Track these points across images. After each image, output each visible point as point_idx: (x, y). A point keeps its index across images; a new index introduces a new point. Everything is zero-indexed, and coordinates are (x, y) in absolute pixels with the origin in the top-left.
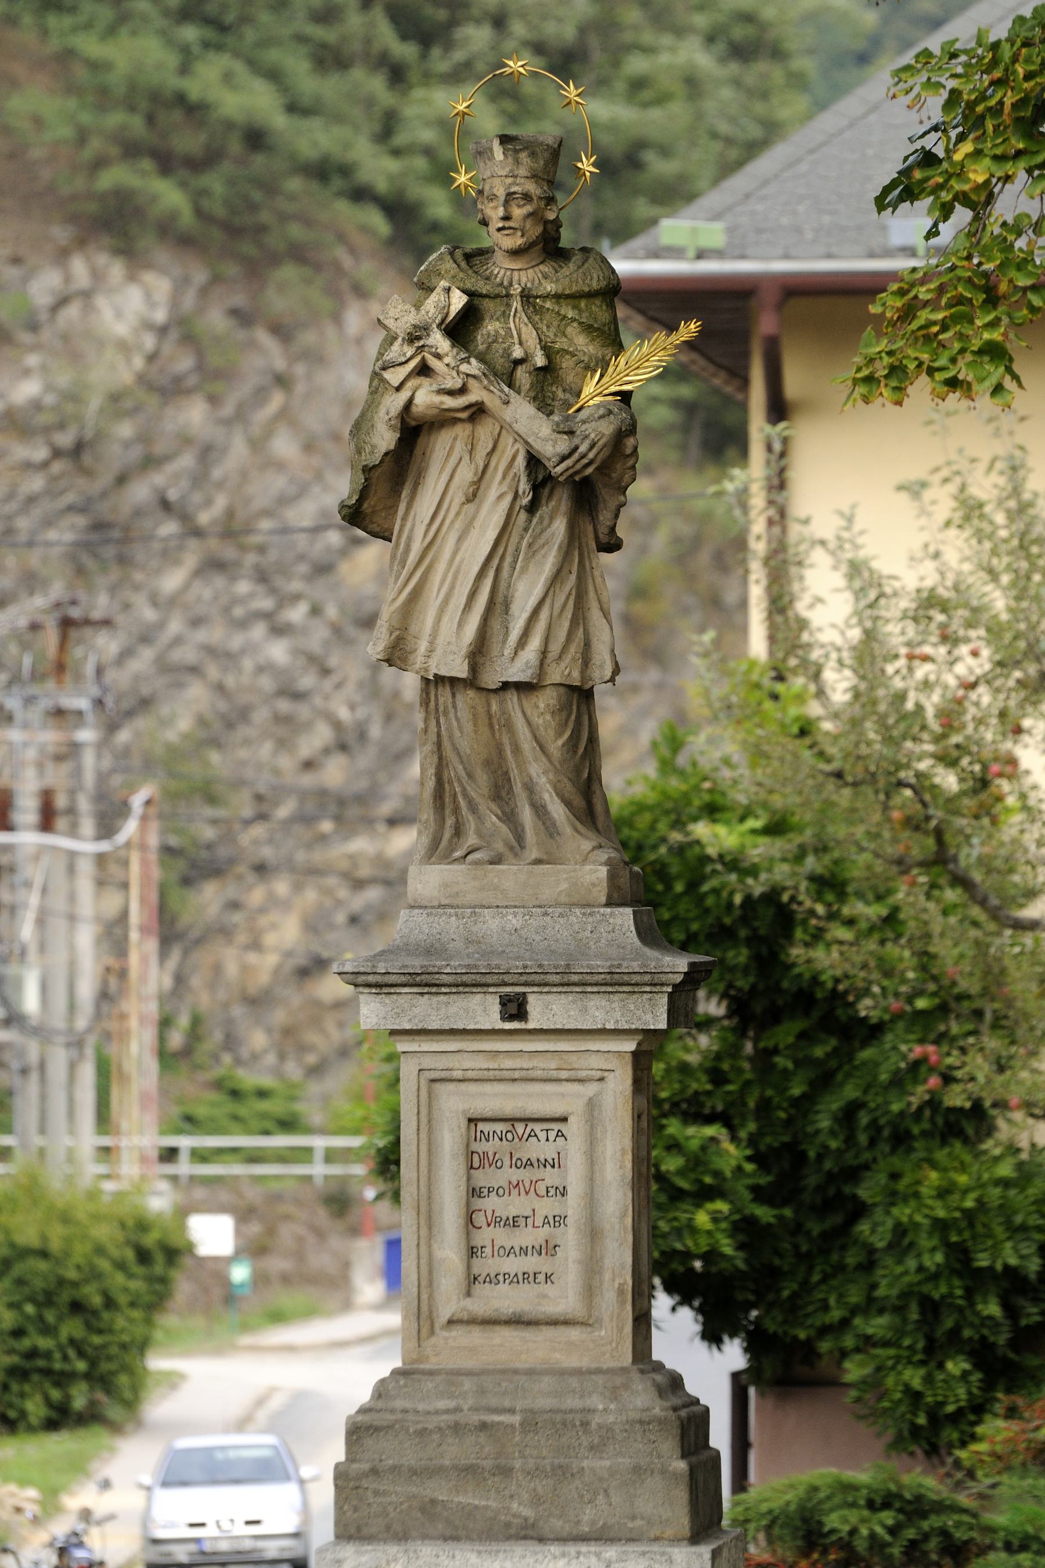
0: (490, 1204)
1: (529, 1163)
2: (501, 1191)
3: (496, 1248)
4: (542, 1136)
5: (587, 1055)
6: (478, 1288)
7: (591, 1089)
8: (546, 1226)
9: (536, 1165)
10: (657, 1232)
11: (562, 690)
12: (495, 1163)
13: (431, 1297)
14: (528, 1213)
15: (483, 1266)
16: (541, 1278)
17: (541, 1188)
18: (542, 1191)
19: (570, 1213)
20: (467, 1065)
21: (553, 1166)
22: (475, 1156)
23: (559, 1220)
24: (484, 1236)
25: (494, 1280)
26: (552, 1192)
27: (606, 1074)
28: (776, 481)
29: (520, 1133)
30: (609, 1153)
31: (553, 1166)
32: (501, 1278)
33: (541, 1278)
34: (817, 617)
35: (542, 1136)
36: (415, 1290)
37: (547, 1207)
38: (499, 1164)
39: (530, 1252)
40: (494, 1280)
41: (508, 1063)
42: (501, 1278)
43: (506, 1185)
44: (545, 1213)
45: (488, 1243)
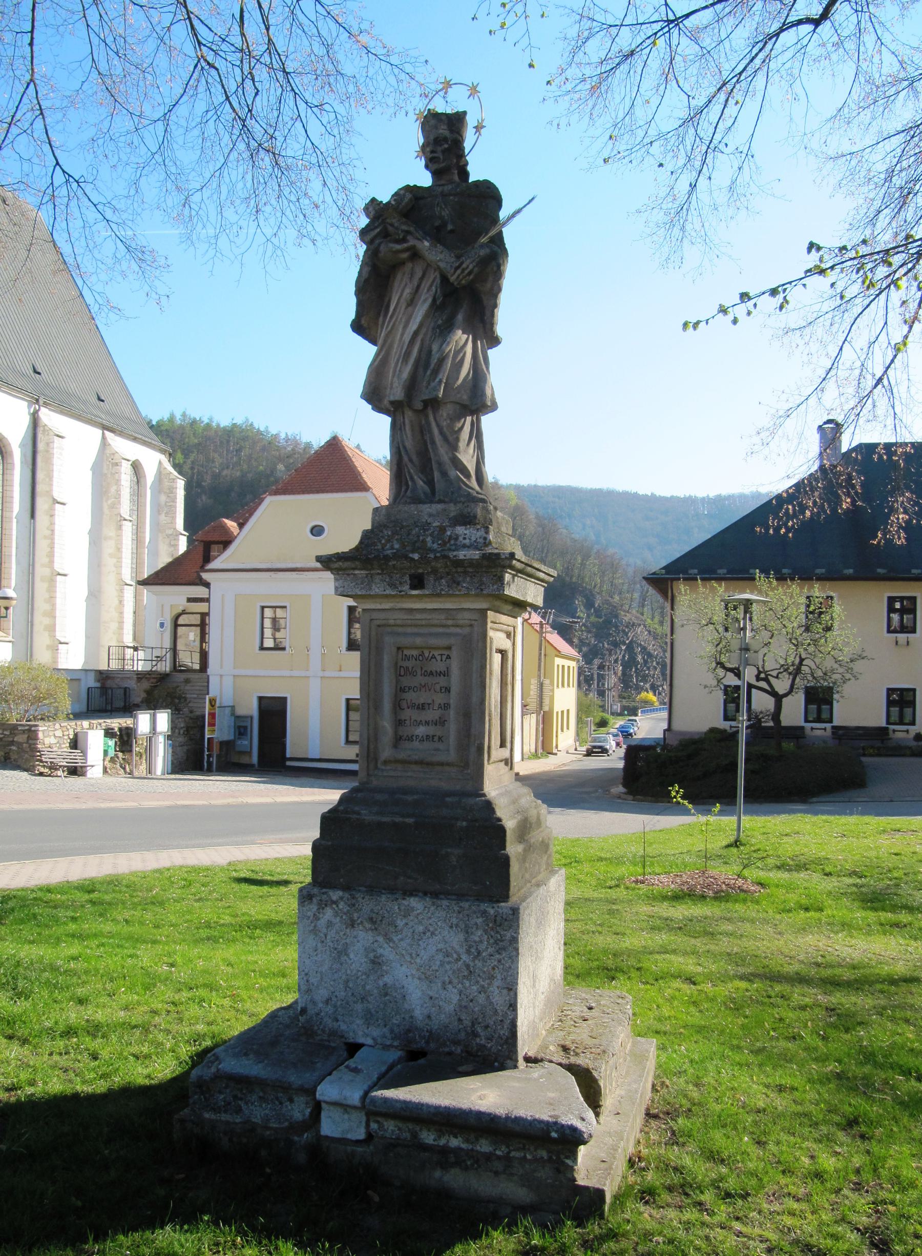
0: (410, 696)
1: (431, 673)
4: (439, 658)
10: (215, 548)
11: (458, 407)
12: (413, 673)
14: (430, 702)
15: (405, 731)
16: (436, 739)
17: (438, 687)
18: (438, 689)
19: (452, 701)
22: (402, 670)
23: (446, 706)
24: (407, 714)
28: (710, 936)
30: (474, 668)
33: (436, 739)
35: (439, 658)
37: (439, 699)
41: (418, 616)
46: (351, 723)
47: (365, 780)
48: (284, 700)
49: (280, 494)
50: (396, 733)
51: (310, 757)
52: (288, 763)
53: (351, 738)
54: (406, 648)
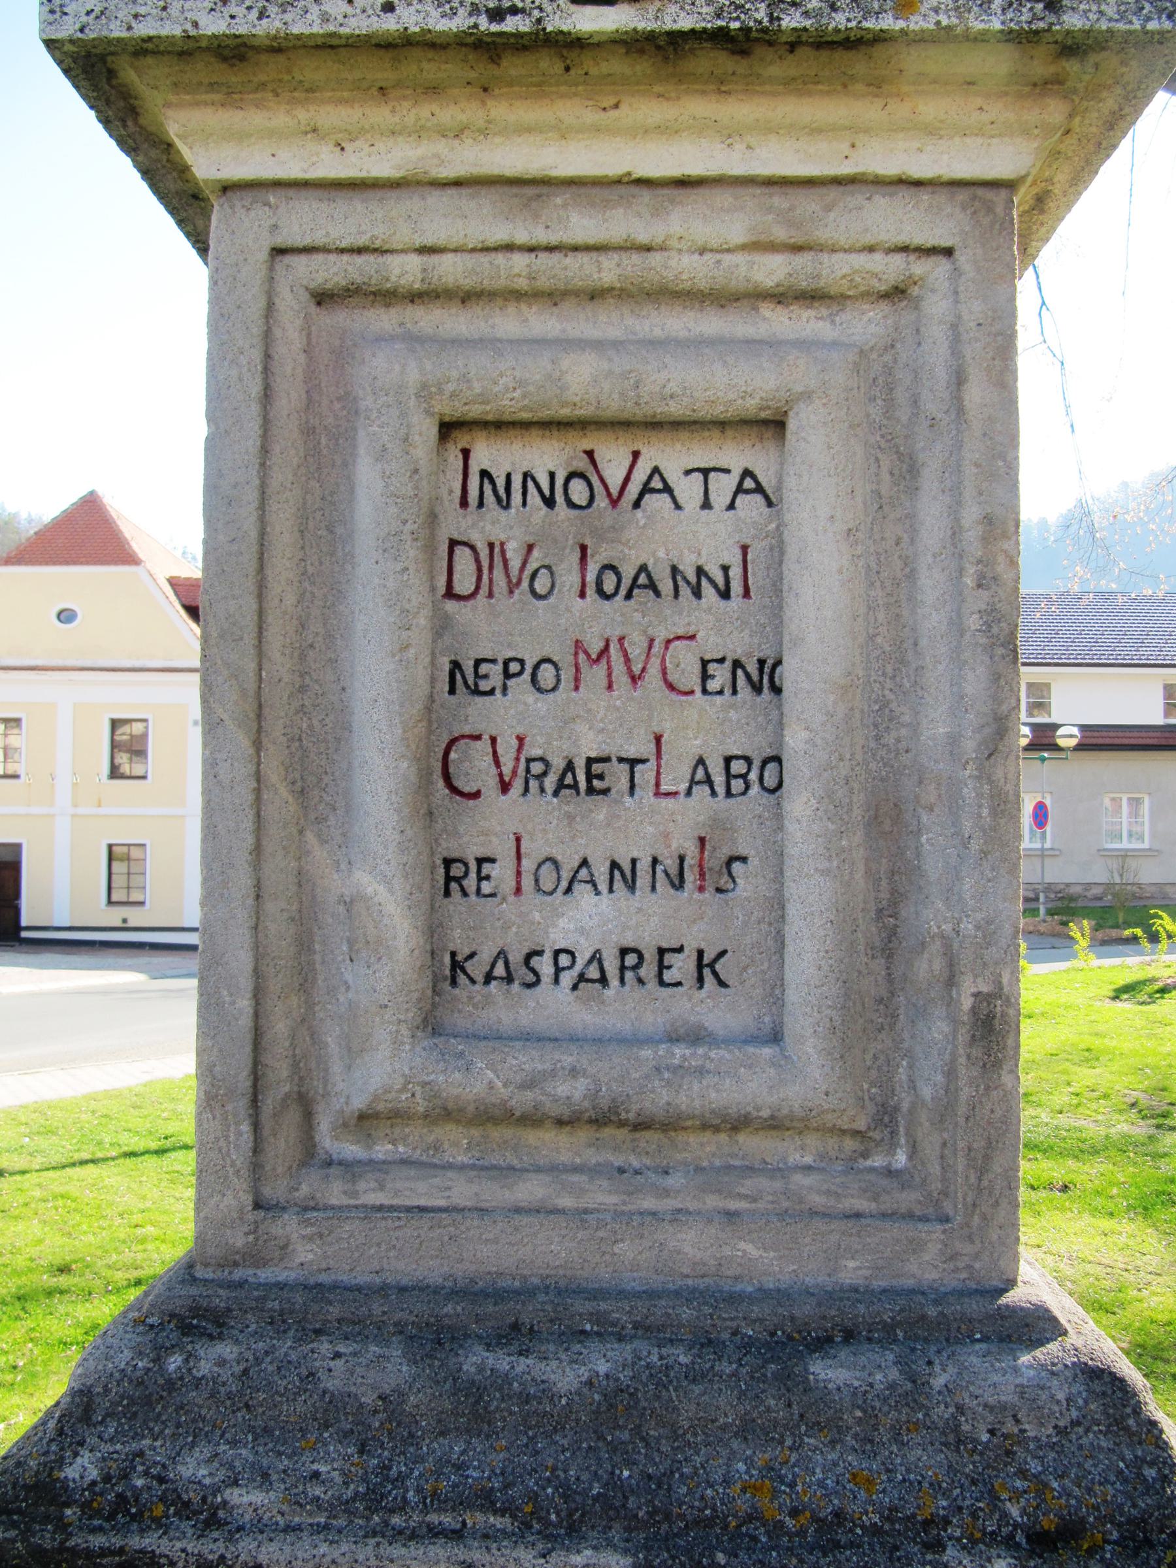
2: (547, 674)
3: (528, 865)
4: (689, 490)
5: (856, 198)
6: (625, 767)
7: (698, 689)
8: (702, 791)
9: (666, 586)
13: (306, 1022)
14: (640, 747)
16: (681, 967)
19: (795, 740)
20: (437, 231)
21: (725, 594)
25: (521, 973)
26: (720, 677)
27: (919, 267)
29: (615, 478)
31: (725, 594)
32: (545, 966)
33: (681, 967)
34: (273, 1547)
35: (689, 490)
36: (245, 1004)
38: (541, 585)
39: (643, 880)
40: (521, 973)
42: (545, 966)
43: (565, 659)
44: (695, 746)
45: (503, 850)
46: (114, 877)
47: (239, 1239)
48: (17, 848)
49: (13, 564)
50: (434, 930)
51: (56, 924)
52: (24, 934)
53: (114, 898)
54: (499, 426)
